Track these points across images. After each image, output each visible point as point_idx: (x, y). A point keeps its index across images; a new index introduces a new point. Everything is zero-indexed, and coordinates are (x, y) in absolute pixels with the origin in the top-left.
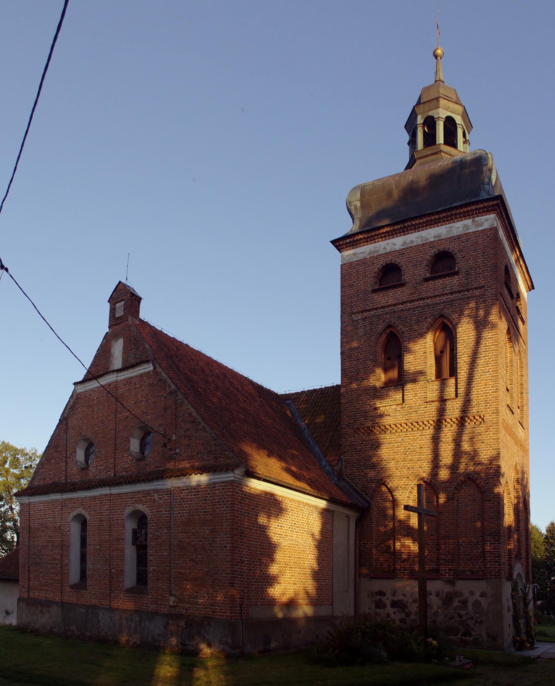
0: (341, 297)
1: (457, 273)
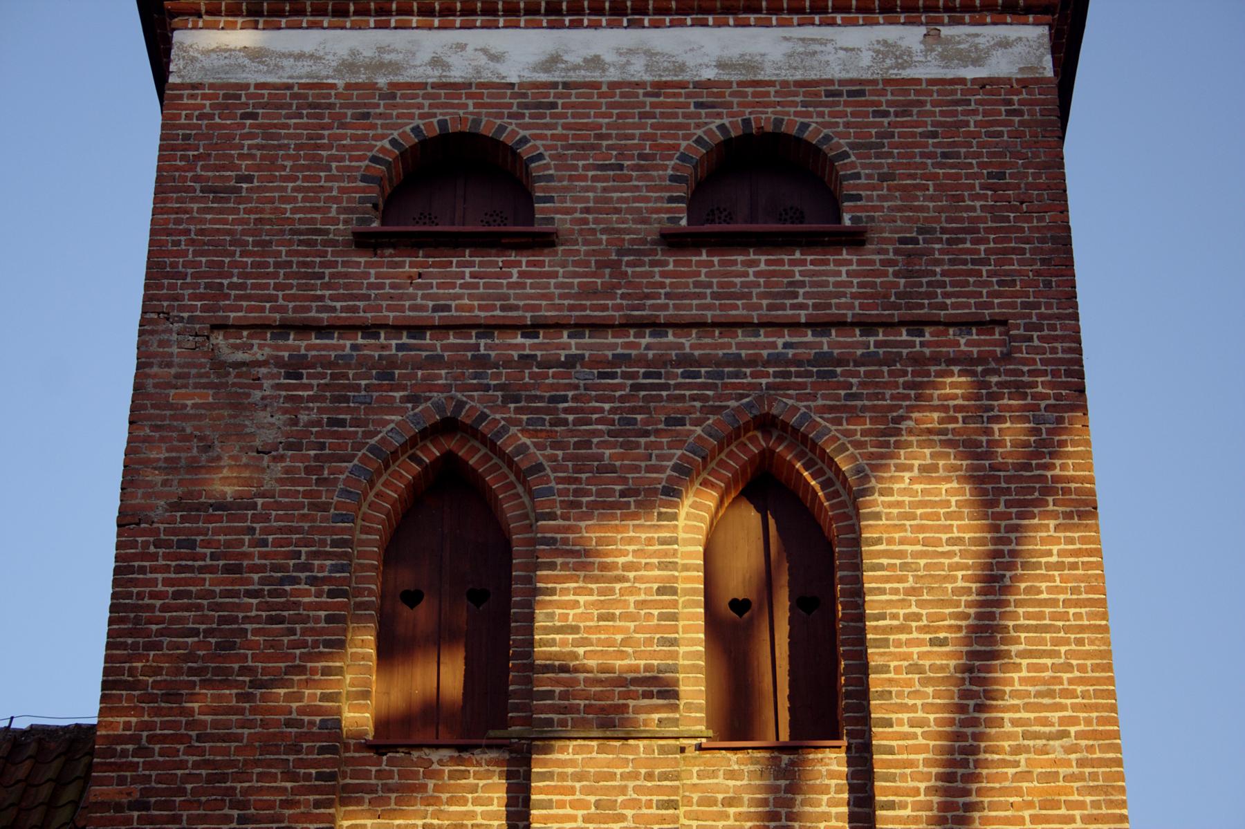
0: (153, 232)
1: (855, 239)
